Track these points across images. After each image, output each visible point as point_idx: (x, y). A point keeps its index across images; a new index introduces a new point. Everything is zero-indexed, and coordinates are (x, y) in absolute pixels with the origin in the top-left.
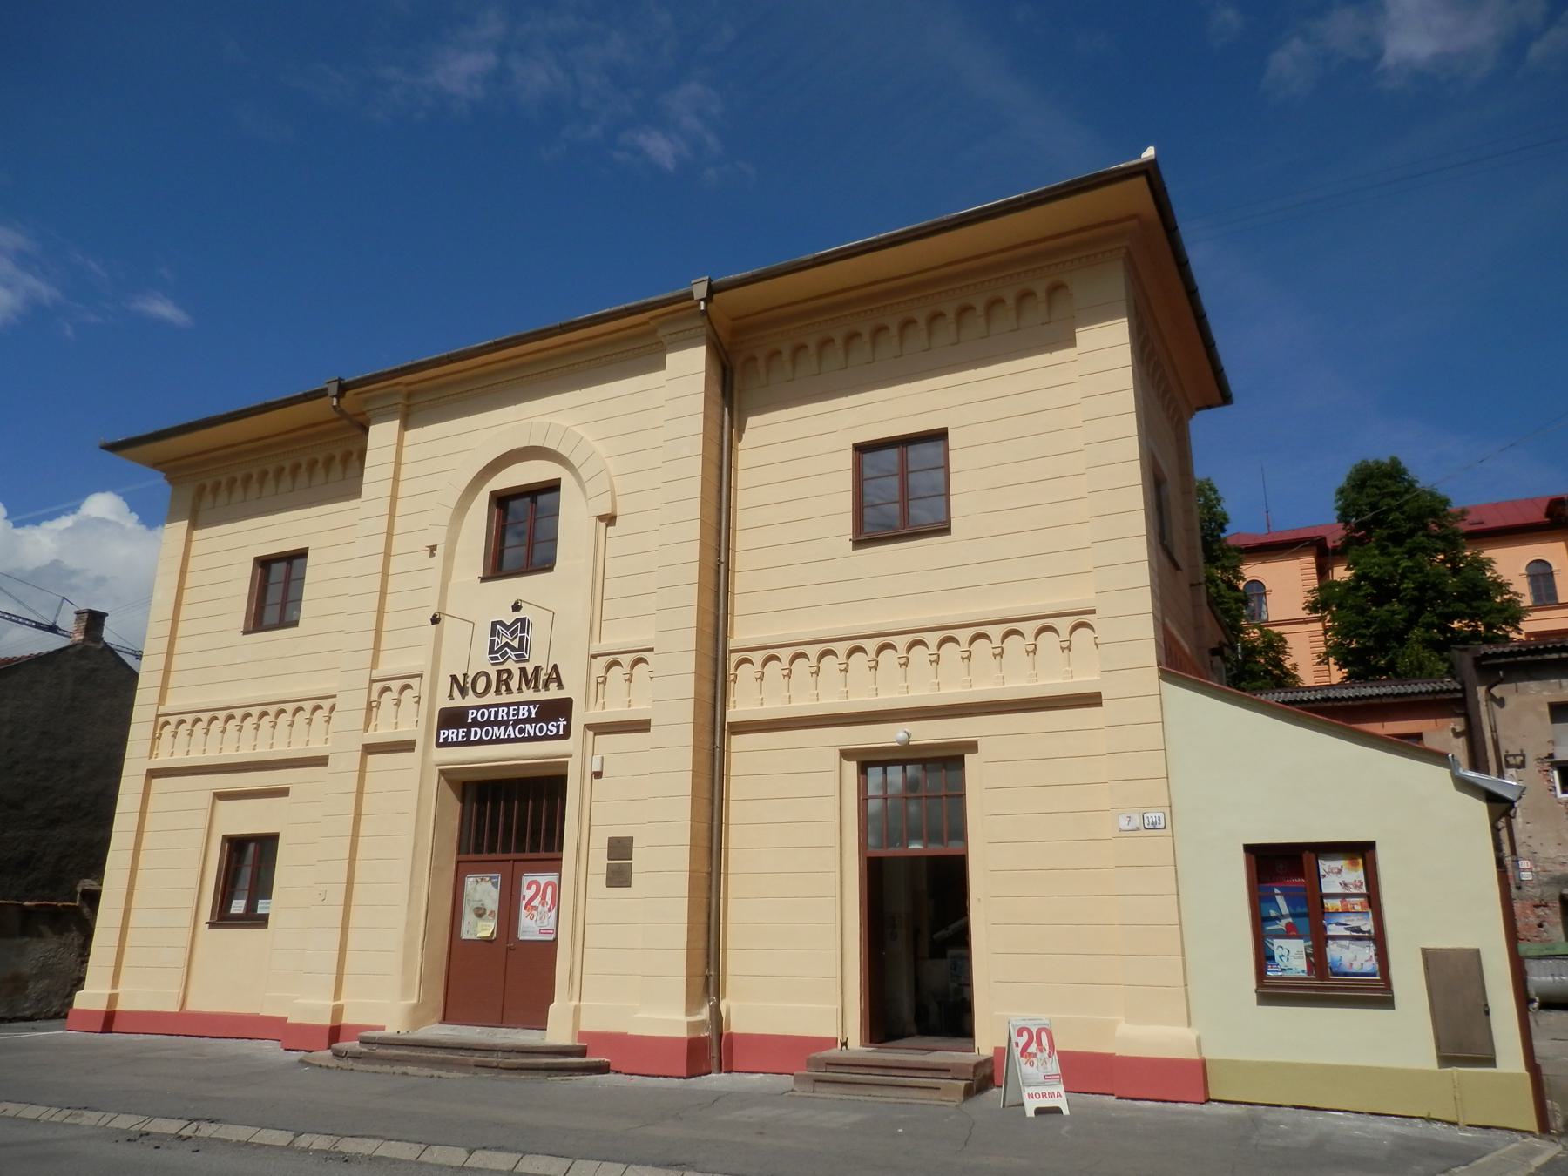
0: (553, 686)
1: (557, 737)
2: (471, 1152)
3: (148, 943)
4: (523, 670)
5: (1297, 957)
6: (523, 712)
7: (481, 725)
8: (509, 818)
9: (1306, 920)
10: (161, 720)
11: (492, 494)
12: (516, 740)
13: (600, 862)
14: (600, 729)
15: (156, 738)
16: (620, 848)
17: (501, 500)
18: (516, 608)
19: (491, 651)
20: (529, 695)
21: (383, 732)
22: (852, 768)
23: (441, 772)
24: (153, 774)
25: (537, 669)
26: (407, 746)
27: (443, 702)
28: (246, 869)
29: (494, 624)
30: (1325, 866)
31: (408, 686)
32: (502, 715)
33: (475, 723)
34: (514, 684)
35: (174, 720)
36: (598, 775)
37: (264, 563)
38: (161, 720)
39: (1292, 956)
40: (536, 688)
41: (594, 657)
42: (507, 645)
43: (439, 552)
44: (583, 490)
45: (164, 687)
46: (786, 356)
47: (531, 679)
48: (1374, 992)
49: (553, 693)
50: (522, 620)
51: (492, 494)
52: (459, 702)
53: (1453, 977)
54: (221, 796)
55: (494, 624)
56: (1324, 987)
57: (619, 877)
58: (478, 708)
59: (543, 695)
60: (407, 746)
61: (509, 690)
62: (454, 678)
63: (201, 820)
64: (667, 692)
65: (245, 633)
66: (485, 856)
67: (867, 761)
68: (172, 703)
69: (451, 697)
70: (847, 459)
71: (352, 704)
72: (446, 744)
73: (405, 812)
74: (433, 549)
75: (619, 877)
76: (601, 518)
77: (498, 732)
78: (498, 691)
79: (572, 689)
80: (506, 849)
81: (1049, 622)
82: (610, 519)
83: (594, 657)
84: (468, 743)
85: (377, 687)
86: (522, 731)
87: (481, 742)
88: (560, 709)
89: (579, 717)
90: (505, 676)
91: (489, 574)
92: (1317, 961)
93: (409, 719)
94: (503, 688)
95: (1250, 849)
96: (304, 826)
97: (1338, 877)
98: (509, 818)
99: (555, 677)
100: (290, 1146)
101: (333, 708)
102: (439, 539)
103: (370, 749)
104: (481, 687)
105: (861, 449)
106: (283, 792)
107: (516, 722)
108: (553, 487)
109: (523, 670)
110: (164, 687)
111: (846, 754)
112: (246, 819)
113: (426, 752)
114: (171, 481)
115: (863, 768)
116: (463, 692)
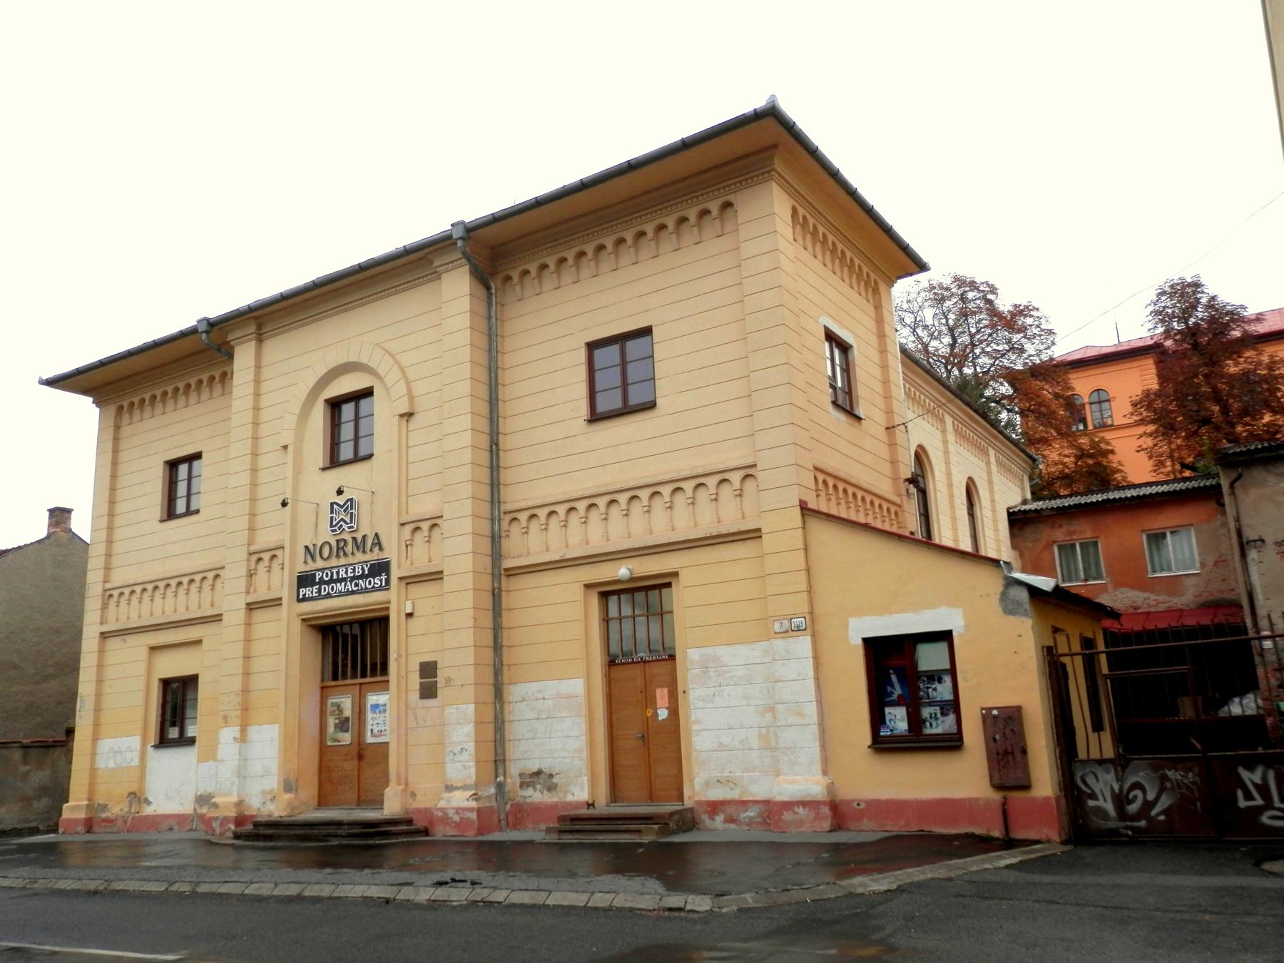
0: (376, 549)
1: (381, 589)
2: (276, 885)
3: (115, 759)
4: (354, 539)
5: (901, 720)
6: (359, 572)
7: (328, 583)
8: (353, 649)
10: (108, 593)
11: (327, 401)
12: (353, 592)
13: (415, 681)
14: (408, 581)
15: (105, 607)
16: (428, 670)
17: (335, 405)
18: (340, 492)
19: (331, 526)
20: (360, 557)
21: (261, 594)
22: (594, 601)
23: (304, 620)
24: (104, 636)
25: (364, 537)
26: (276, 602)
27: (301, 568)
28: (177, 700)
29: (332, 504)
31: (274, 556)
32: (342, 574)
33: (322, 582)
34: (349, 549)
35: (116, 593)
36: (410, 615)
37: (173, 465)
38: (108, 593)
40: (364, 552)
41: (403, 525)
43: (290, 449)
44: (389, 395)
45: (108, 568)
46: (571, 261)
47: (360, 545)
48: (952, 743)
49: (375, 556)
52: (311, 566)
53: (1005, 730)
54: (153, 649)
55: (332, 504)
56: (917, 741)
57: (428, 691)
58: (322, 570)
59: (368, 557)
60: (276, 602)
61: (345, 555)
62: (307, 547)
63: (141, 669)
64: (458, 550)
65: (162, 521)
66: (340, 682)
67: (606, 593)
68: (118, 578)
69: (305, 562)
70: (582, 355)
71: (235, 574)
72: (304, 599)
73: (283, 649)
74: (285, 447)
75: (428, 691)
76: (402, 416)
77: (340, 587)
78: (338, 556)
79: (391, 552)
80: (354, 676)
81: (727, 476)
82: (409, 415)
83: (403, 525)
85: (255, 557)
87: (329, 596)
88: (381, 568)
89: (395, 573)
90: (342, 544)
91: (328, 465)
92: (916, 722)
93: (280, 583)
94: (341, 553)
96: (214, 664)
97: (930, 658)
98: (353, 649)
99: (378, 543)
100: (194, 893)
102: (288, 438)
103: (251, 607)
104: (326, 552)
105: (592, 346)
106: (198, 642)
108: (368, 393)
109: (354, 539)
110: (108, 568)
111: (588, 586)
112: (175, 665)
113: (289, 607)
114: (98, 403)
115: (605, 596)
116: (313, 558)
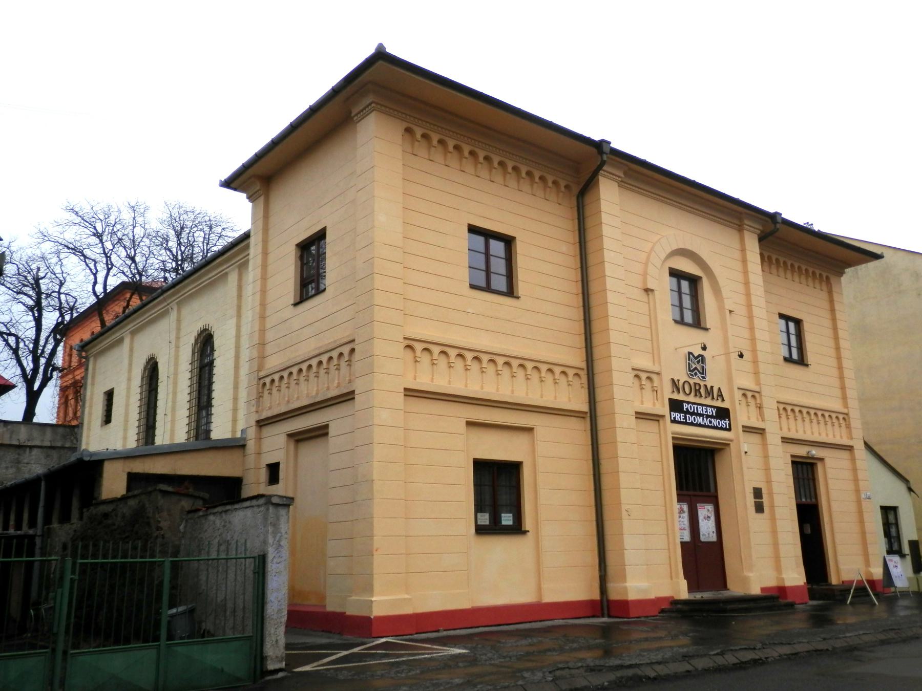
1: (725, 429)
9: (18, 416)
11: (701, 278)
30: (710, 507)
32: (700, 411)
33: (687, 412)
39: (484, 519)
42: (696, 368)
50: (702, 356)
51: (701, 278)
77: (699, 420)
84: (686, 423)
86: (710, 422)
95: (521, 463)
101: (353, 350)
107: (708, 416)
109: (706, 386)
